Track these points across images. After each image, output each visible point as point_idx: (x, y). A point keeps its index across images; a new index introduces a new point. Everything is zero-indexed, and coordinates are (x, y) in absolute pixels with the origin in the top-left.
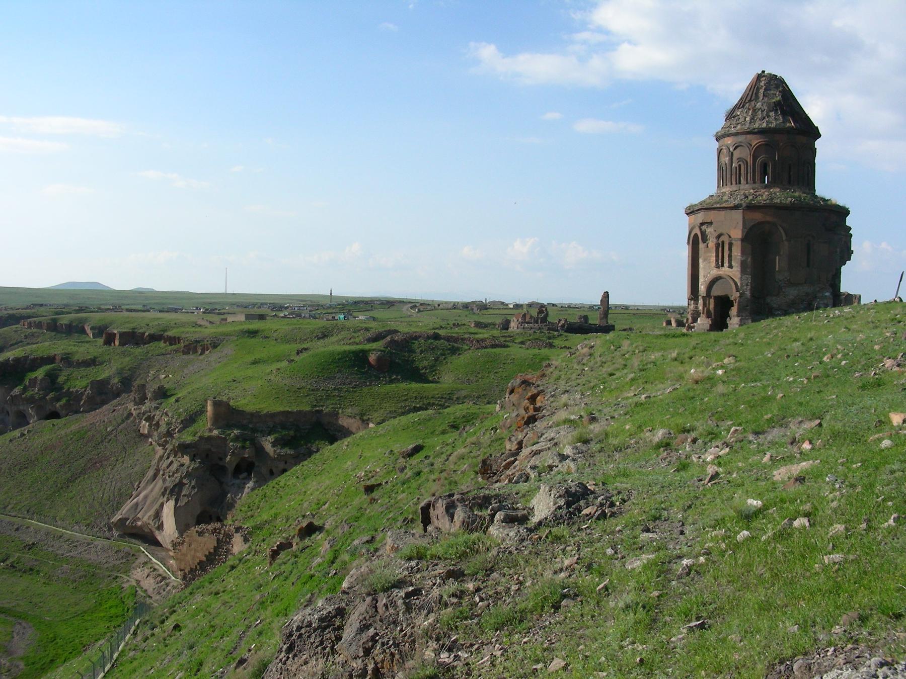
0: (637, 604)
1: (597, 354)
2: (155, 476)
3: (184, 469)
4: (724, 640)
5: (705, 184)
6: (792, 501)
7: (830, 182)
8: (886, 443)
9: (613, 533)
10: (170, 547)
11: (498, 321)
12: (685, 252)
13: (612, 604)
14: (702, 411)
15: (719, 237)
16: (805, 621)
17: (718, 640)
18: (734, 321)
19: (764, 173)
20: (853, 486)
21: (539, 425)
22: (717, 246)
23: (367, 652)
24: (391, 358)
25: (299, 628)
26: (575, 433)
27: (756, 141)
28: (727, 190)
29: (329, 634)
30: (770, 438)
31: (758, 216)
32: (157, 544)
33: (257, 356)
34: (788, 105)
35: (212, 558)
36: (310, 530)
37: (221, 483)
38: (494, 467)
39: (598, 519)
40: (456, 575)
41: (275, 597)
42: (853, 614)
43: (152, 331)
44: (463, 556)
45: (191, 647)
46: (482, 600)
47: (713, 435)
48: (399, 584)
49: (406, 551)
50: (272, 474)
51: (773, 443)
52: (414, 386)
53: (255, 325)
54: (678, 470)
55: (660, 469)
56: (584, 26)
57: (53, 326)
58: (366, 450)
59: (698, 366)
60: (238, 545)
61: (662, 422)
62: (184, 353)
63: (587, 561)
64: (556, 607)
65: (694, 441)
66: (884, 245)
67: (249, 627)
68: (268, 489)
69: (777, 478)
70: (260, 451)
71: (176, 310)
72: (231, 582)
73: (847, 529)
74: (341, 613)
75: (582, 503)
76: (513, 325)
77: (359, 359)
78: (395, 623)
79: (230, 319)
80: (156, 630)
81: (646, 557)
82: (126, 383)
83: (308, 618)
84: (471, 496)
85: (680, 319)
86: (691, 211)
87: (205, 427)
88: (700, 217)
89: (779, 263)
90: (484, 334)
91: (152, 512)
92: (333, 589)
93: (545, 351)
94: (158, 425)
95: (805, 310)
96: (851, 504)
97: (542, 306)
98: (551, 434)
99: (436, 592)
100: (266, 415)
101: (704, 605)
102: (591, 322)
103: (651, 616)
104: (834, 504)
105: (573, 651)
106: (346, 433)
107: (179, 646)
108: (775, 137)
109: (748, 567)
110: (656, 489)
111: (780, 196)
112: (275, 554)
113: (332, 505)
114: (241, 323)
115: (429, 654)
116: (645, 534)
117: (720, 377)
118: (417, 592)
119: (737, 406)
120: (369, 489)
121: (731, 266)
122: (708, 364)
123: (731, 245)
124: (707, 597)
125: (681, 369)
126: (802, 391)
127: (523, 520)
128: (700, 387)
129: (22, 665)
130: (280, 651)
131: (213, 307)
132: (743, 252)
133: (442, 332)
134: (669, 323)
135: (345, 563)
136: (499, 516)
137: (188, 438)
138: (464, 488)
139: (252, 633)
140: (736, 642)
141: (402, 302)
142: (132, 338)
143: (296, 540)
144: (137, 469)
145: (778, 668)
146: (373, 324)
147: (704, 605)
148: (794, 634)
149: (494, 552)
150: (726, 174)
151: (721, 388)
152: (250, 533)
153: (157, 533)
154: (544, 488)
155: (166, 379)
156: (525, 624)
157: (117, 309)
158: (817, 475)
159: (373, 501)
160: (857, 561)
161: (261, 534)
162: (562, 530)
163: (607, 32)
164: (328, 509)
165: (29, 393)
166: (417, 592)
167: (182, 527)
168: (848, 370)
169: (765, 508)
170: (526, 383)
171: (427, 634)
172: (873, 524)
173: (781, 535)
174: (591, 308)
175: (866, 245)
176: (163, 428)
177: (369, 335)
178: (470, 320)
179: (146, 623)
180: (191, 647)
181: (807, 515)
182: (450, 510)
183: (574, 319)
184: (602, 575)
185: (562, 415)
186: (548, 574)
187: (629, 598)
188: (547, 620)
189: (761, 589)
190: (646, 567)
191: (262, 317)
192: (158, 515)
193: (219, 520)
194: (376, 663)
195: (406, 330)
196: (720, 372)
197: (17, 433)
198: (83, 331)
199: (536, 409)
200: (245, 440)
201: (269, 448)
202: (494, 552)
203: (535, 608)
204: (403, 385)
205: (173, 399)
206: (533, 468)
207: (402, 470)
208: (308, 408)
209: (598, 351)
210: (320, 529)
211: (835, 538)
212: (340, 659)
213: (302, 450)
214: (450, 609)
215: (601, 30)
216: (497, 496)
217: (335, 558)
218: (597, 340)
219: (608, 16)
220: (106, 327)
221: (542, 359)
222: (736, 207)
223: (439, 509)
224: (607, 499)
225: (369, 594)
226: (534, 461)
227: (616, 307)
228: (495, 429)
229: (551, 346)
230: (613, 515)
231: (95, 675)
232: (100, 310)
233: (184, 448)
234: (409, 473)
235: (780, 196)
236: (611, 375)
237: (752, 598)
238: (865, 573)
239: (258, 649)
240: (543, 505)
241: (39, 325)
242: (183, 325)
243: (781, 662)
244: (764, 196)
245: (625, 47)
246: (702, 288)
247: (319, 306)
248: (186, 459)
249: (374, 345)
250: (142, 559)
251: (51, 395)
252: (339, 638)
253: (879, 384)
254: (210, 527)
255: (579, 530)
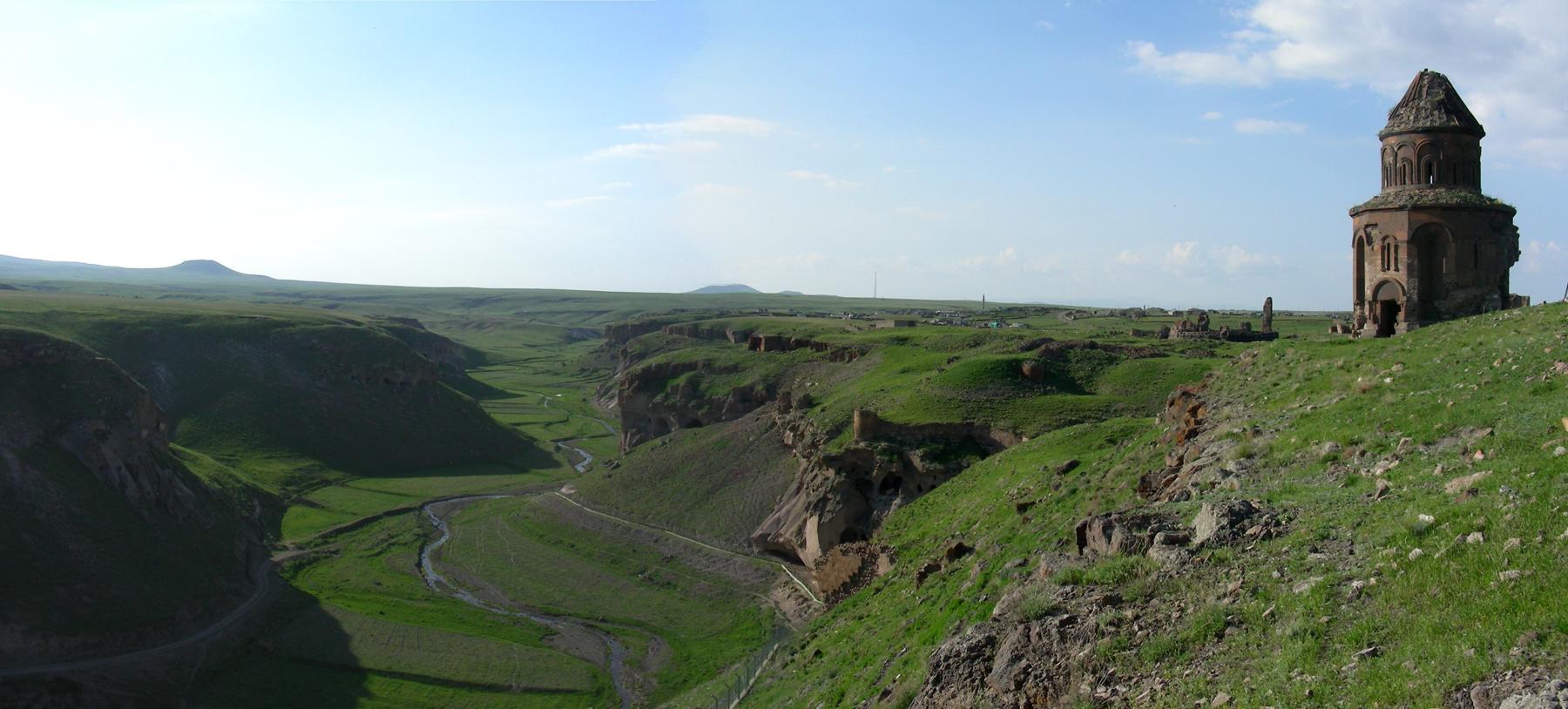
0: (1305, 631)
1: (1260, 364)
2: (799, 490)
3: (829, 483)
4: (1397, 668)
5: (1369, 185)
6: (1465, 515)
7: (1497, 179)
8: (1560, 450)
9: (1279, 554)
10: (812, 566)
11: (1157, 329)
12: (1349, 255)
13: (1279, 632)
14: (1370, 422)
15: (1384, 239)
16: (1482, 644)
17: (1391, 667)
18: (1401, 327)
19: (1430, 173)
20: (1527, 497)
21: (1201, 439)
22: (1383, 248)
23: (1019, 685)
24: (1046, 367)
25: (947, 658)
26: (1238, 447)
27: (1420, 140)
28: (1392, 190)
29: (979, 665)
30: (1441, 448)
31: (1424, 217)
32: (799, 562)
33: (907, 365)
34: (1452, 103)
35: (856, 580)
36: (960, 551)
37: (867, 499)
38: (1154, 485)
39: (1263, 539)
40: (1113, 601)
41: (923, 624)
42: (1531, 634)
43: (799, 337)
44: (1121, 581)
45: (833, 676)
46: (1141, 628)
47: (1382, 447)
48: (1053, 611)
49: (1061, 575)
50: (920, 490)
51: (1444, 454)
52: (1069, 397)
53: (905, 332)
54: (1346, 486)
55: (1328, 485)
56: (1244, 24)
57: (695, 333)
58: (1019, 467)
59: (1365, 374)
60: (883, 566)
61: (1329, 434)
62: (832, 360)
63: (1252, 585)
64: (1220, 636)
65: (1363, 454)
66: (1551, 245)
67: (894, 655)
68: (917, 505)
69: (1449, 491)
70: (908, 465)
71: (823, 315)
72: (875, 605)
73: (1522, 543)
74: (991, 642)
75: (1246, 522)
76: (1173, 333)
77: (1013, 368)
78: (1049, 653)
79: (879, 325)
80: (797, 656)
81: (1315, 580)
82: (771, 391)
83: (957, 647)
84: (1129, 515)
85: (1345, 326)
86: (1355, 213)
87: (851, 439)
88: (1365, 219)
89: (1446, 265)
90: (1143, 343)
91: (794, 528)
92: (983, 617)
93: (1207, 361)
94: (802, 435)
95: (1474, 313)
96: (1526, 516)
97: (1203, 313)
98: (1213, 449)
99: (1092, 620)
100: (915, 427)
101: (1376, 630)
102: (1254, 329)
103: (1320, 644)
104: (1509, 517)
105: (1238, 684)
106: (998, 447)
107: (820, 674)
108: (1439, 135)
109: (1421, 587)
110: (1323, 506)
111: (1445, 196)
112: (922, 577)
113: (983, 524)
114: (890, 330)
115: (1085, 688)
116: (1313, 555)
117: (1388, 386)
118: (1072, 620)
119: (1406, 416)
120: (1022, 508)
121: (1397, 270)
122: (1376, 373)
123: (1396, 247)
124: (1379, 621)
125: (1348, 377)
126: (1473, 398)
127: (1184, 541)
128: (1367, 396)
129: (655, 682)
130: (927, 683)
131: (862, 312)
132: (1409, 255)
133: (1099, 341)
134: (1334, 329)
135: (996, 588)
136: (1159, 537)
137: (833, 450)
138: (1121, 507)
139: (897, 662)
140: (1410, 669)
141: (1057, 309)
142: (778, 343)
143: (945, 561)
144: (779, 481)
145: (1454, 696)
146: (1027, 332)
147: (1376, 630)
148: (1471, 658)
149: (1154, 576)
150: (1391, 174)
151: (1389, 397)
152: (896, 554)
153: (799, 551)
154: (1206, 507)
155: (811, 387)
156: (1187, 655)
157: (763, 312)
158: (1490, 486)
159: (1026, 520)
160: (1533, 576)
161: (908, 555)
162: (1225, 552)
163: (1267, 31)
164: (979, 530)
165: (672, 400)
166: (1072, 620)
167: (826, 546)
168: (1518, 376)
169: (1437, 523)
170: (1186, 394)
171: (1083, 666)
172: (1549, 536)
173: (1455, 551)
174: (1254, 314)
175: (1534, 245)
176: (808, 439)
177: (1023, 343)
178: (1128, 328)
179: (785, 648)
180: (833, 676)
181: (1481, 529)
182: (1107, 530)
183: (1237, 326)
184: (1268, 600)
185: (1225, 428)
186: (1211, 600)
187: (1297, 624)
188: (1210, 649)
189: (1434, 611)
190: (1313, 590)
191: (912, 324)
192: (800, 531)
193: (864, 538)
194: (1028, 698)
195: (1061, 338)
196: (1388, 380)
197: (658, 441)
198: (724, 336)
199: (1197, 423)
200: (892, 453)
201: (917, 462)
202: (1154, 576)
203: (1197, 637)
204: (1058, 397)
205: (818, 409)
206: (1195, 485)
207: (1057, 487)
208: (959, 421)
209: (1262, 360)
210: (970, 550)
211: (1510, 553)
212: (990, 693)
213: (952, 465)
214: (1107, 639)
215: (1262, 29)
216: (1156, 515)
217: (986, 582)
218: (1260, 349)
219: (1269, 15)
220: (752, 331)
221: (1204, 369)
222: (1401, 208)
223: (1096, 530)
224: (1272, 517)
225: (1021, 622)
226: (1196, 478)
227: (1280, 313)
228: (1154, 443)
229: (1213, 355)
230: (1279, 534)
231: (729, 702)
232: (741, 314)
233: (829, 461)
234: (1064, 491)
235: (1445, 196)
236: (1276, 385)
237: (1426, 620)
238: (1542, 588)
239: (903, 680)
240: (1205, 525)
241: (680, 331)
242: (830, 331)
243: (1458, 690)
244: (1429, 196)
245: (1286, 45)
246: (1368, 293)
247: (971, 313)
248: (831, 473)
249: (1028, 354)
250: (784, 579)
251: (693, 403)
252: (989, 670)
253: (1550, 388)
254: (855, 546)
255: (1244, 551)
